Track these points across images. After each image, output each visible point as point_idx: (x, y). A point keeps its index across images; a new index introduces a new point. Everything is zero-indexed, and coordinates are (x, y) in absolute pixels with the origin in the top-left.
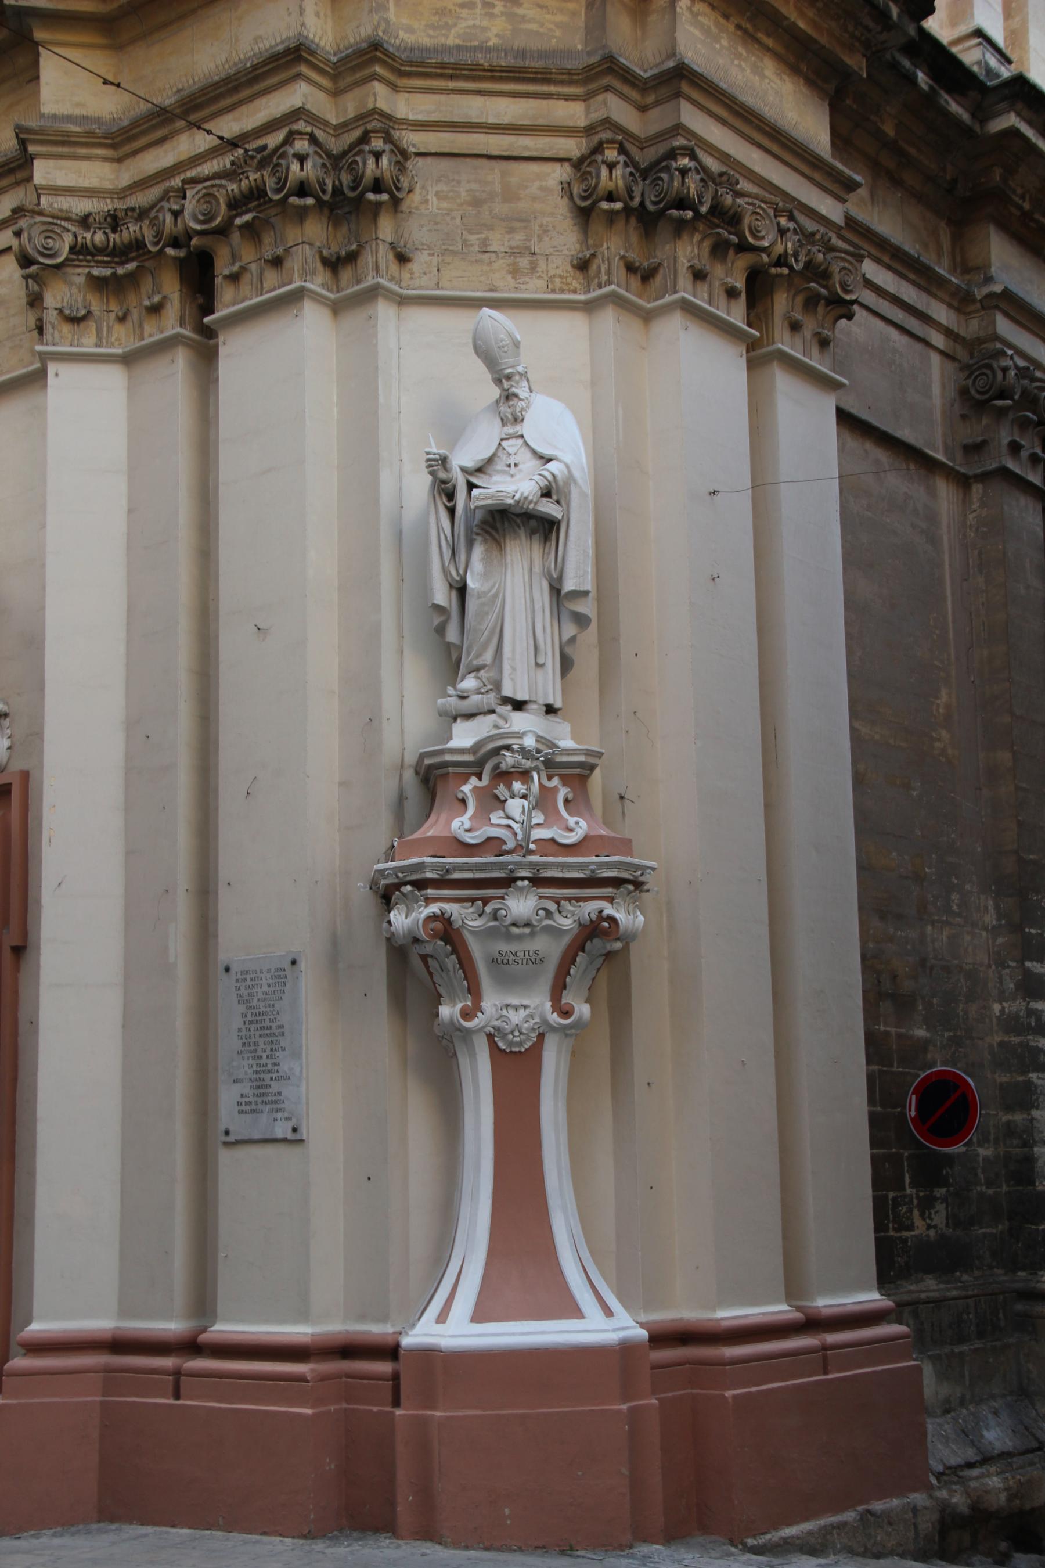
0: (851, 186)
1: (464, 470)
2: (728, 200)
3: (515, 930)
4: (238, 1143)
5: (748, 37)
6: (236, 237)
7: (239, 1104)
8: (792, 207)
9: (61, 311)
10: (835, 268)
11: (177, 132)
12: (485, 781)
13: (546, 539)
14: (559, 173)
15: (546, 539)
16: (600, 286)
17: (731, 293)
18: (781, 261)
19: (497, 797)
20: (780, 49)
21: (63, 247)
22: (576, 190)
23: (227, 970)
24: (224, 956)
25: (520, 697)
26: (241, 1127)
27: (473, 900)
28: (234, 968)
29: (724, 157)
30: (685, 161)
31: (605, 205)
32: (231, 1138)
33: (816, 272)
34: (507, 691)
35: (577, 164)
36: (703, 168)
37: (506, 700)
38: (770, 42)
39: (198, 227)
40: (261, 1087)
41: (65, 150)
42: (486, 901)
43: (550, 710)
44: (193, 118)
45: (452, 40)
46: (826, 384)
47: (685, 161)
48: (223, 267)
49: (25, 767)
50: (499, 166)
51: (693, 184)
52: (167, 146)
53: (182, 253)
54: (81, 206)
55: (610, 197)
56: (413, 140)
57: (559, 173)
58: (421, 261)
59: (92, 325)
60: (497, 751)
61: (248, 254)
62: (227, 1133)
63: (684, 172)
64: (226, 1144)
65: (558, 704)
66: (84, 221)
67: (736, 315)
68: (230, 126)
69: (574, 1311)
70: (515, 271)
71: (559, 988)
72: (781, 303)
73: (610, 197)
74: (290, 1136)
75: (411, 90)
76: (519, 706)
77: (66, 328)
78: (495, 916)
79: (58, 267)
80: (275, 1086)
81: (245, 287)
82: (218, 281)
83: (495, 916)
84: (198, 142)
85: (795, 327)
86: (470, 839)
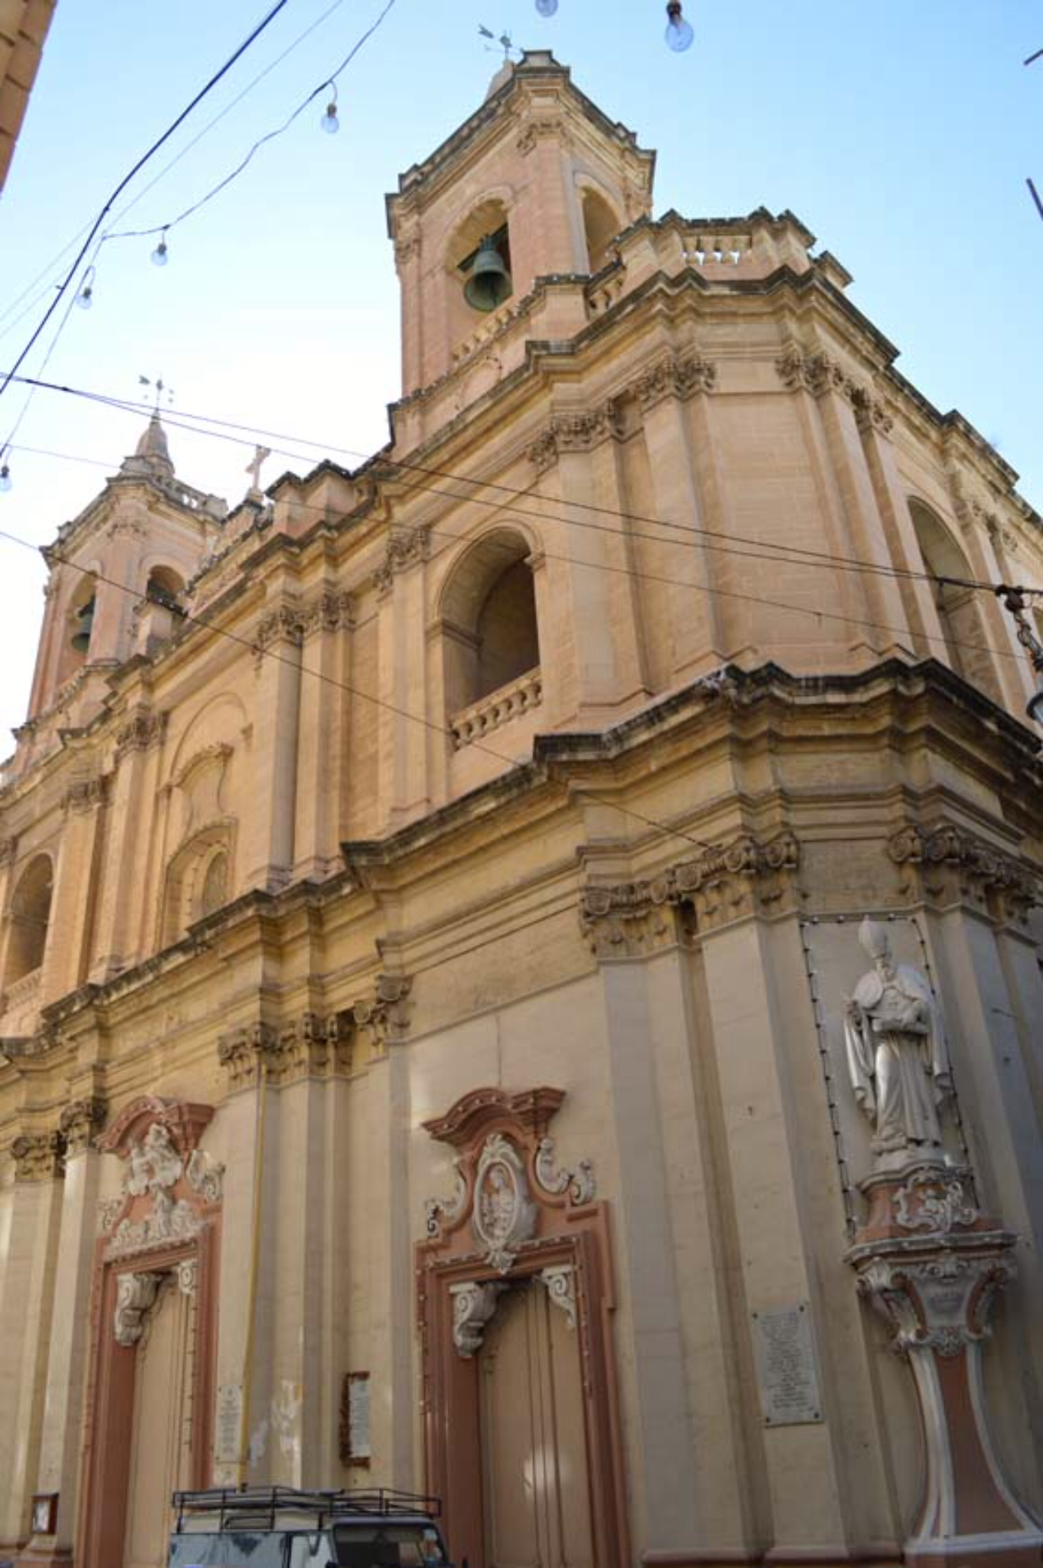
0: (1019, 837)
1: (865, 1009)
2: (972, 851)
3: (945, 1281)
4: (774, 1426)
5: (960, 768)
6: (708, 892)
7: (775, 1401)
8: (1001, 853)
9: (606, 938)
10: (1023, 880)
11: (664, 842)
12: (909, 1190)
13: (919, 1045)
14: (878, 846)
15: (919, 1045)
16: (915, 902)
17: (980, 900)
18: (999, 880)
19: (919, 1199)
20: (972, 772)
21: (607, 904)
22: (892, 851)
23: (755, 1316)
24: (751, 1305)
25: (921, 1137)
26: (777, 1416)
27: (917, 1264)
28: (761, 1314)
29: (965, 830)
30: (951, 834)
31: (912, 860)
32: (771, 1423)
33: (1015, 884)
34: (911, 1135)
35: (891, 839)
36: (958, 837)
37: (911, 1140)
38: (967, 769)
39: (686, 889)
40: (788, 1389)
41: (603, 856)
42: (925, 1263)
43: (936, 1144)
44: (680, 832)
45: (813, 784)
46: (1031, 943)
47: (951, 834)
48: (700, 905)
49: (605, 1198)
50: (848, 844)
51: (956, 845)
52: (662, 847)
53: (675, 903)
54: (612, 883)
55: (913, 855)
56: (801, 835)
57: (878, 846)
58: (814, 897)
59: (623, 944)
60: (915, 1171)
61: (714, 898)
62: (768, 1420)
63: (951, 839)
64: (767, 1427)
65: (939, 1140)
66: (615, 890)
67: (983, 910)
68: (699, 835)
69: (1017, 1525)
70: (865, 898)
71: (971, 1314)
72: (1001, 902)
73: (913, 855)
74: (814, 1420)
75: (797, 810)
76: (919, 1143)
77: (611, 947)
78: (932, 1271)
79: (604, 916)
80: (798, 1388)
81: (716, 917)
82: (699, 915)
83: (932, 1271)
84: (682, 843)
85: (1010, 914)
86: (911, 1225)
